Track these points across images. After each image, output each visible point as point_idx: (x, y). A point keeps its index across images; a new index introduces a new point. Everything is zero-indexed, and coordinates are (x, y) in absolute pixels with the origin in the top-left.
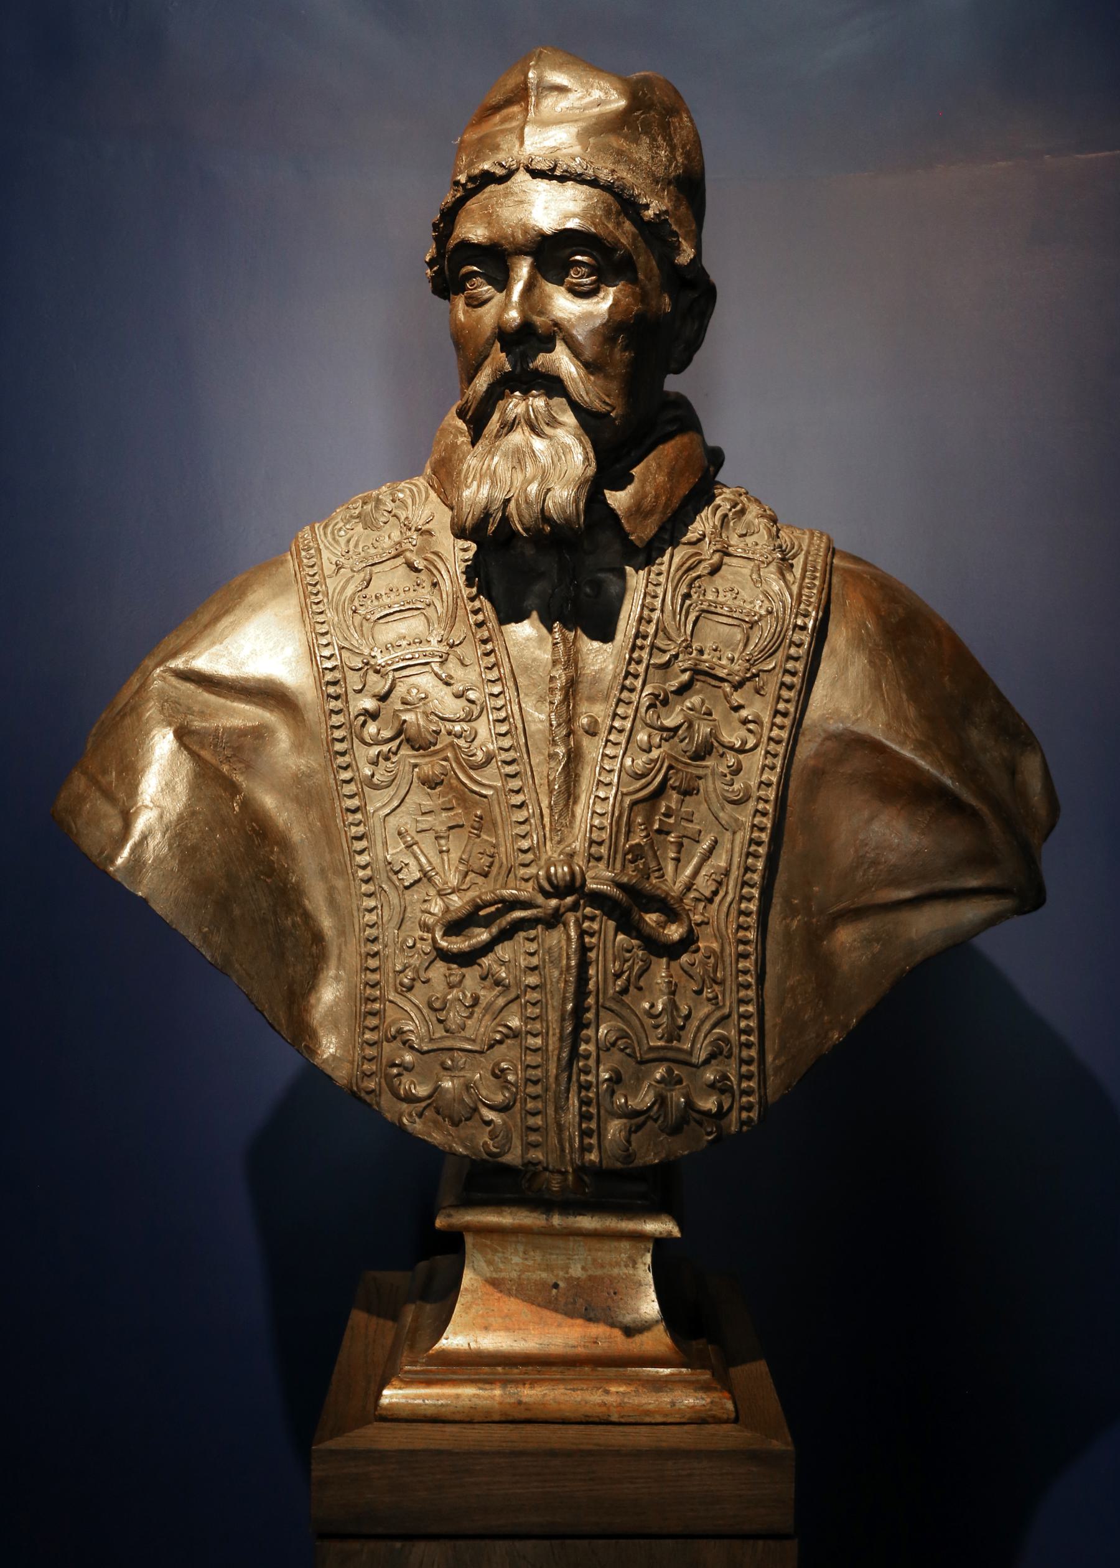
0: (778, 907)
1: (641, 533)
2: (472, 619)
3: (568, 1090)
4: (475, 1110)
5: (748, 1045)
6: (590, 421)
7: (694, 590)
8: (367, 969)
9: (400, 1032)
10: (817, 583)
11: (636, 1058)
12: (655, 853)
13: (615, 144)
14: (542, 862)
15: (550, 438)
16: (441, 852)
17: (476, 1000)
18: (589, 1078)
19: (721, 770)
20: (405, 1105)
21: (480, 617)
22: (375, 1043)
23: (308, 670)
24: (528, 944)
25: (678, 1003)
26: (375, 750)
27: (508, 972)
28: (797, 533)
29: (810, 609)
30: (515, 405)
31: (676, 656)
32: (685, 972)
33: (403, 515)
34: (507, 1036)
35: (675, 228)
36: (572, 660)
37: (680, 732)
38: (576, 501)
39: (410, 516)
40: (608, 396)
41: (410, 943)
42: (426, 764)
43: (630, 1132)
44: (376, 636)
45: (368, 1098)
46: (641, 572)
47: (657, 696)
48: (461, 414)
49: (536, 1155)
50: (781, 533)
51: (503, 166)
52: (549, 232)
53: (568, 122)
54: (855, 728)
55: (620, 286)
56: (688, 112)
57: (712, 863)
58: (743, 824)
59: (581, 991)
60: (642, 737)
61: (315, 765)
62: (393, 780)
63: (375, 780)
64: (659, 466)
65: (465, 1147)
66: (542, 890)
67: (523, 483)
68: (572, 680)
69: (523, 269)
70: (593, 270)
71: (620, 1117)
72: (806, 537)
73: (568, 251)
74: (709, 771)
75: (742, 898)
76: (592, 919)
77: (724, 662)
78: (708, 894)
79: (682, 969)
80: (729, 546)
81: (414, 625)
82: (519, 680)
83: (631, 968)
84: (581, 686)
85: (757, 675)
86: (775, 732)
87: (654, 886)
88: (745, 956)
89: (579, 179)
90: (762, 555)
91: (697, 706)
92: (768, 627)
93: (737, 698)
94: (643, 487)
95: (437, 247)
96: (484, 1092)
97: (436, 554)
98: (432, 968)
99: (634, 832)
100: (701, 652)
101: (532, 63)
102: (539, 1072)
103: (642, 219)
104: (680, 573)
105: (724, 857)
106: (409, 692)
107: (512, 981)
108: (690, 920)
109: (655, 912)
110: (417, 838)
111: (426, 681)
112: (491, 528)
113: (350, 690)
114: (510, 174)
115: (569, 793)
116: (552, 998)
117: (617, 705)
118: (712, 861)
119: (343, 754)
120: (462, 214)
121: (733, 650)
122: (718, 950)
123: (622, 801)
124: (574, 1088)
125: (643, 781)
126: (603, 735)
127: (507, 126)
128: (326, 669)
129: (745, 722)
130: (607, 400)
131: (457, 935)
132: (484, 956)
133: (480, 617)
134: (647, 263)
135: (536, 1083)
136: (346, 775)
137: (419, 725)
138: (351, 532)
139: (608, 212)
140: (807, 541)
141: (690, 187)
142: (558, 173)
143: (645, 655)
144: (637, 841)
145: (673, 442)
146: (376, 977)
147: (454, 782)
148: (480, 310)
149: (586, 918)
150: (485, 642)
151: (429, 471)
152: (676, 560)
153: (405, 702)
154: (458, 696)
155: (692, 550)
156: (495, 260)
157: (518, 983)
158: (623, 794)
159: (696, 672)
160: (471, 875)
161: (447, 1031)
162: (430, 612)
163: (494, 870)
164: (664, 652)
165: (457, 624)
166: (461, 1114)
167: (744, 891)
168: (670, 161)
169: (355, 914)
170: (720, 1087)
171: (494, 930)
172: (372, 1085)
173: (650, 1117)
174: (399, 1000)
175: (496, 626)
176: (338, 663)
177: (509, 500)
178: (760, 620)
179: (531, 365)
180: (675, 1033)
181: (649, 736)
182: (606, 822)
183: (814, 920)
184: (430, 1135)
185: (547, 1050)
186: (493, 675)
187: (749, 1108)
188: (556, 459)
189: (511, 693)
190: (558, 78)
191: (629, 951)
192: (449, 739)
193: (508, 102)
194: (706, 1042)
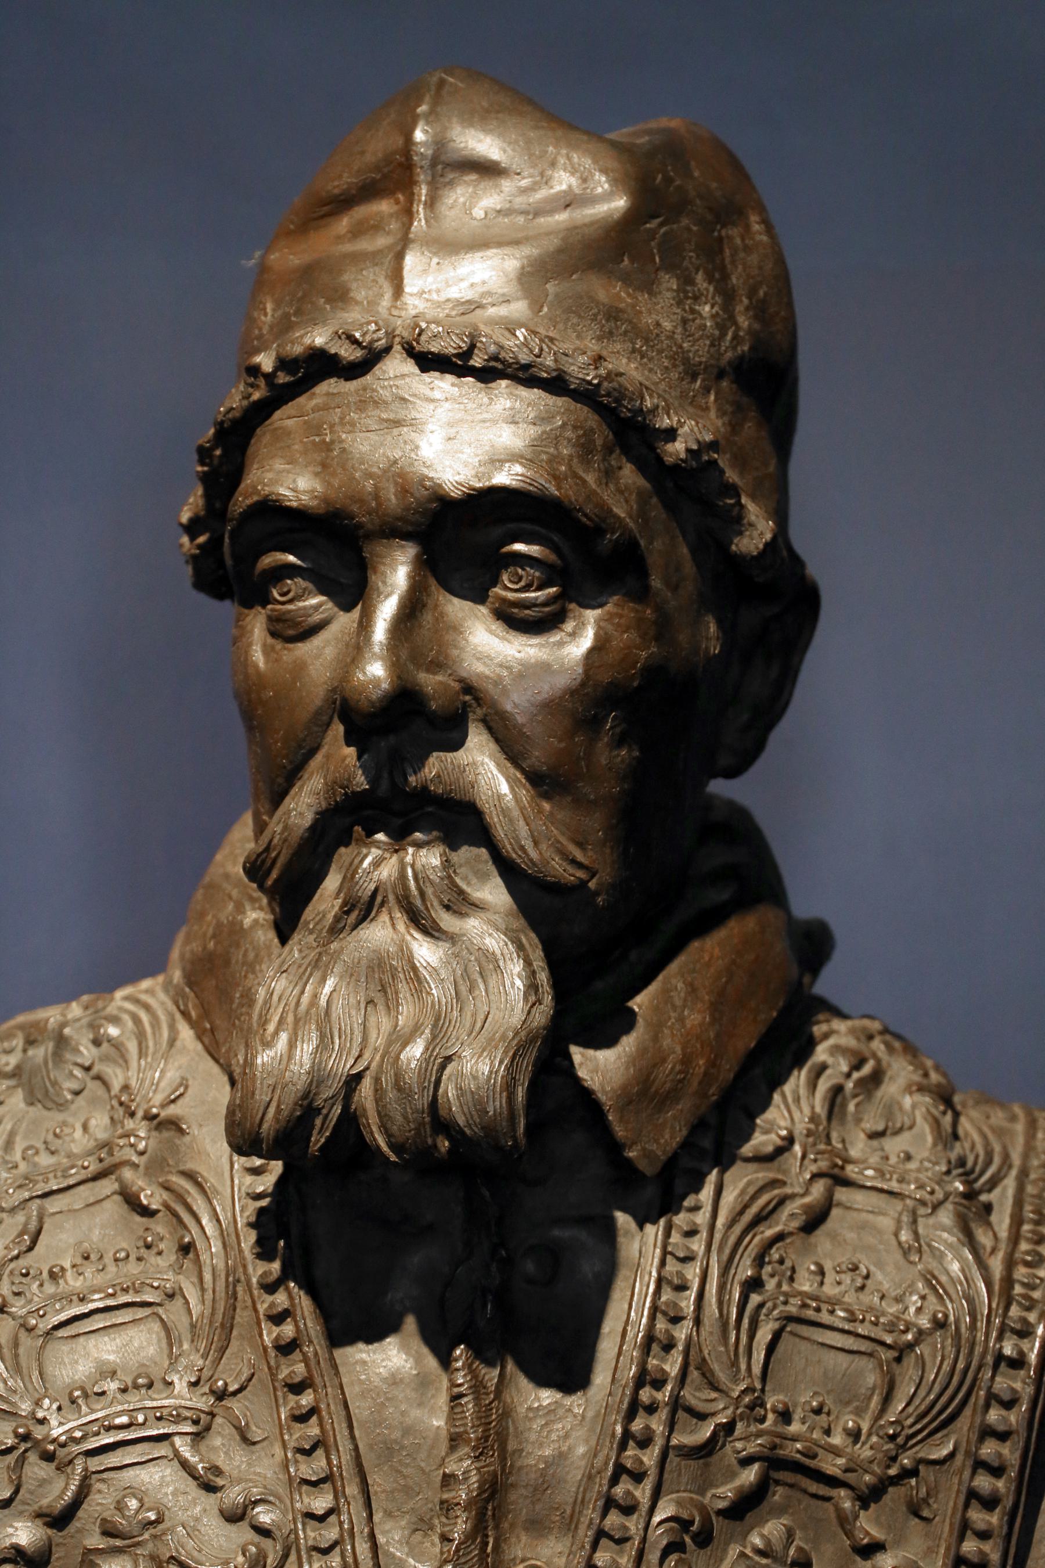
1: (650, 1143)
2: (269, 1334)
6: (539, 901)
7: (768, 1269)
13: (602, 295)
21: (288, 1330)
28: (998, 1117)
29: (1032, 1317)
30: (376, 862)
35: (732, 475)
36: (492, 1435)
38: (509, 1086)
39: (133, 1083)
40: (580, 845)
44: (49, 1369)
46: (650, 1229)
47: (684, 1524)
51: (355, 342)
52: (456, 494)
53: (500, 244)
55: (609, 607)
56: (761, 209)
64: (692, 989)
67: (389, 1043)
68: (494, 1483)
69: (397, 574)
70: (550, 574)
72: (1020, 1127)
73: (497, 531)
80: (847, 1161)
81: (134, 1345)
82: (377, 1480)
84: (513, 1496)
85: (913, 1472)
89: (524, 375)
91: (778, 1547)
92: (936, 1358)
93: (869, 1525)
94: (655, 1039)
95: (208, 496)
97: (190, 1176)
100: (785, 1416)
101: (423, 108)
103: (659, 460)
104: (738, 1229)
106: (120, 1507)
111: (158, 1480)
112: (318, 1140)
114: (372, 358)
120: (263, 440)
121: (859, 1412)
127: (365, 245)
130: (579, 856)
133: (288, 1330)
134: (668, 553)
139: (585, 449)
140: (1020, 1140)
141: (764, 383)
142: (477, 362)
143: (657, 1424)
145: (721, 934)
148: (303, 649)
150: (297, 1388)
151: (177, 975)
153: (109, 1531)
154: (234, 1516)
155: (762, 1174)
156: (337, 545)
159: (774, 1463)
162: (173, 1312)
164: (702, 1417)
168: (722, 328)
177: (358, 1077)
179: (412, 779)
186: (315, 1467)
188: (463, 989)
189: (356, 1510)
190: (484, 144)
193: (369, 191)
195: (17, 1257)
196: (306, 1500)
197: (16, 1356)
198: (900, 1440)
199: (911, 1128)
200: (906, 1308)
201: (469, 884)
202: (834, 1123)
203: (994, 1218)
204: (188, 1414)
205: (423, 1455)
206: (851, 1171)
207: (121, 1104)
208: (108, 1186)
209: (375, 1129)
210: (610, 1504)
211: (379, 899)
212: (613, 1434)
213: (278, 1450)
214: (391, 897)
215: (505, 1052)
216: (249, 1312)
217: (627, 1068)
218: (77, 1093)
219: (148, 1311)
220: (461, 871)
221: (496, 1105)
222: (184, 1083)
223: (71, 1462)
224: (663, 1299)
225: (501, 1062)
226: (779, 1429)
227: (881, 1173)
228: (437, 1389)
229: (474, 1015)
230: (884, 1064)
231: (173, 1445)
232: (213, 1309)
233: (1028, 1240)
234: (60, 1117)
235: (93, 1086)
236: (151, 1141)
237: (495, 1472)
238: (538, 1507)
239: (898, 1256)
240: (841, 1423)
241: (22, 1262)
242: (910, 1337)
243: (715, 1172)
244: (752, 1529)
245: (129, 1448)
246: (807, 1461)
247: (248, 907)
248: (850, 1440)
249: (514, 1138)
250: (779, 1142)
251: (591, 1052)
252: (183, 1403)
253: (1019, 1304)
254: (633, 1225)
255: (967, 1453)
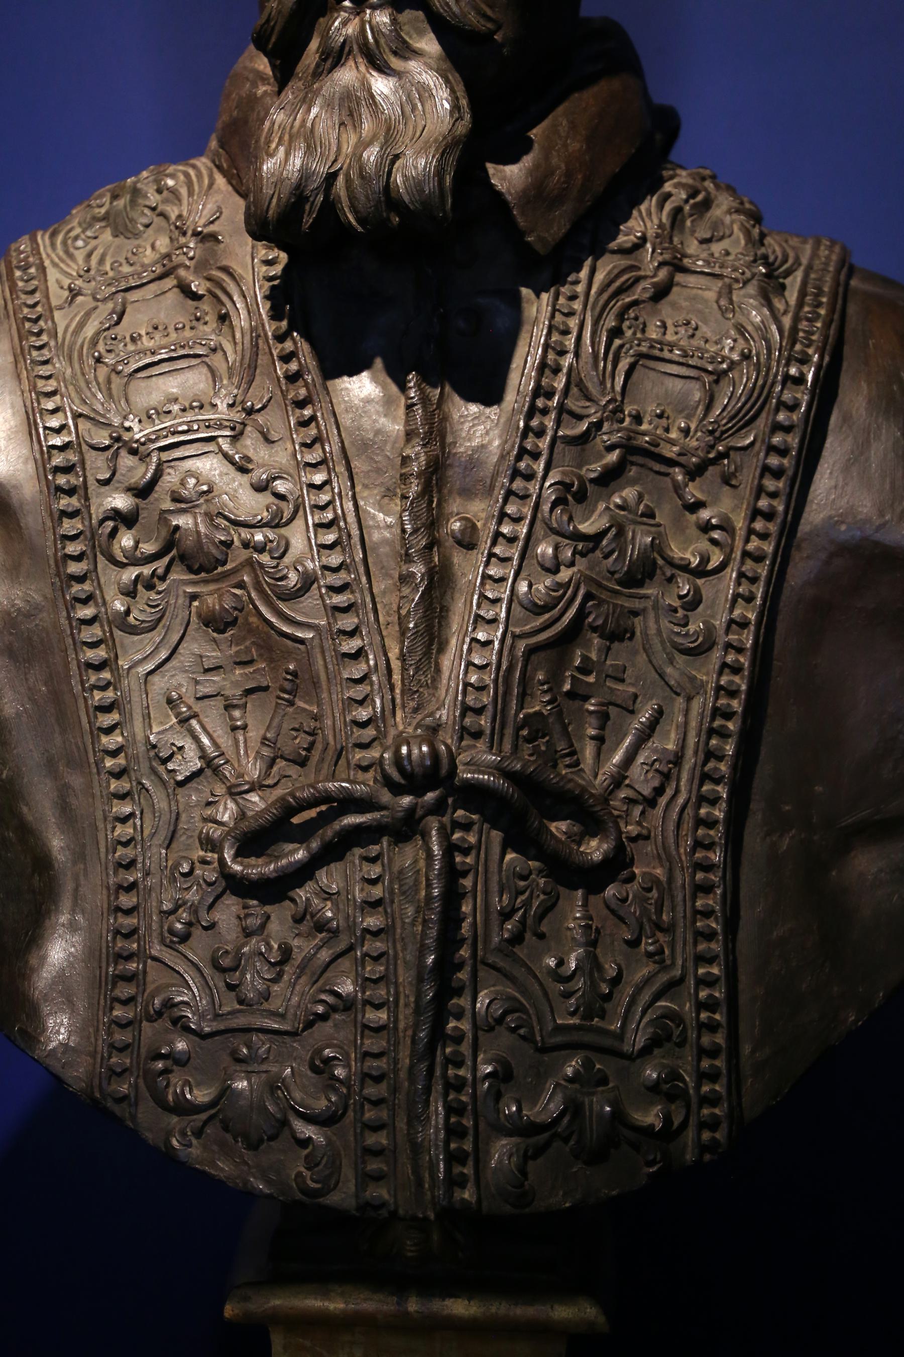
0: (759, 816)
1: (545, 232)
3: (428, 1090)
4: (284, 1123)
5: (712, 1027)
7: (627, 323)
8: (118, 909)
9: (169, 1004)
10: (822, 312)
11: (535, 1042)
12: (565, 727)
14: (390, 741)
15: (397, 74)
16: (234, 729)
17: (286, 953)
18: (461, 1072)
19: (668, 601)
20: (175, 1119)
21: (294, 366)
22: (130, 1023)
23: (26, 451)
24: (366, 866)
25: (601, 960)
26: (130, 574)
27: (336, 909)
28: (794, 241)
29: (810, 351)
31: (598, 425)
32: (613, 912)
33: (173, 214)
34: (333, 1009)
36: (435, 431)
37: (604, 542)
38: (440, 173)
39: (185, 213)
40: (491, 7)
41: (185, 868)
42: (211, 594)
43: (526, 1158)
44: (132, 398)
45: (117, 1109)
46: (545, 296)
48: (261, 44)
49: (381, 1192)
50: (768, 240)
54: (878, 537)
57: (651, 747)
58: (703, 685)
59: (449, 939)
60: (545, 549)
61: (37, 598)
62: (159, 620)
63: (131, 619)
64: (573, 126)
65: (268, 1182)
66: (388, 782)
67: (356, 147)
71: (510, 1134)
74: (649, 604)
75: (702, 799)
76: (466, 827)
77: (673, 435)
78: (647, 791)
79: (608, 907)
80: (685, 256)
81: (189, 382)
82: (355, 463)
83: (527, 904)
84: (450, 473)
86: (754, 544)
87: (563, 777)
88: (706, 889)
90: (735, 270)
92: (744, 380)
96: (298, 1095)
98: (219, 905)
99: (532, 695)
100: (638, 419)
102: (382, 1064)
104: (605, 296)
105: (673, 735)
106: (183, 483)
107: (342, 923)
108: (620, 832)
109: (565, 819)
110: (197, 707)
111: (209, 466)
112: (308, 221)
113: (91, 481)
115: (431, 634)
116: (404, 949)
117: (506, 501)
118: (655, 743)
119: (81, 579)
121: (689, 417)
122: (663, 879)
123: (513, 647)
124: (438, 1087)
125: (547, 616)
126: (485, 546)
128: (54, 447)
129: (706, 528)
130: (489, 12)
131: (258, 856)
132: (300, 887)
133: (294, 366)
135: (378, 1079)
136: (87, 612)
137: (198, 533)
138: (93, 243)
143: (550, 423)
144: (537, 708)
145: (595, 89)
146: (130, 922)
147: (253, 620)
149: (457, 825)
150: (301, 404)
151: (213, 144)
152: (600, 277)
153: (177, 498)
154: (260, 488)
155: (623, 262)
157: (351, 927)
158: (515, 637)
159: (631, 450)
160: (281, 763)
161: (241, 1002)
162: (217, 360)
163: (316, 755)
164: (580, 418)
165: (258, 378)
166: (262, 1130)
167: (705, 788)
169: (101, 825)
170: (667, 1090)
171: (315, 845)
172: (124, 1089)
173: (556, 1135)
174: (168, 956)
175: (319, 381)
176: (73, 437)
177: (335, 175)
178: (730, 369)
180: (596, 1006)
181: (556, 548)
182: (488, 678)
183: (816, 838)
184: (213, 1164)
185: (396, 1028)
186: (313, 456)
187: (713, 1124)
188: (408, 109)
189: (340, 483)
191: (524, 878)
192: (244, 554)
194: (645, 1020)
195: (108, 329)
196: (309, 476)
197: (109, 389)
198: (717, 434)
199: (730, 236)
200: (723, 348)
201: (410, 37)
202: (676, 232)
203: (787, 293)
204: (227, 424)
205: (388, 448)
206: (686, 262)
207: (177, 227)
208: (170, 282)
209: (346, 210)
210: (516, 473)
211: (347, 49)
212: (518, 427)
213: (289, 446)
214: (355, 47)
215: (437, 150)
216: (268, 356)
217: (527, 177)
218: (147, 226)
219: (198, 361)
220: (406, 28)
221: (430, 187)
222: (219, 210)
223: (149, 454)
224: (553, 339)
225: (433, 157)
226: (634, 427)
227: (707, 263)
228: (398, 406)
229: (415, 127)
230: (713, 196)
231: (218, 444)
232: (243, 356)
233: (809, 305)
234: (136, 242)
235: (158, 221)
236: (198, 251)
237: (437, 456)
238: (467, 480)
239: (719, 315)
240: (677, 424)
241: (111, 331)
242: (725, 366)
243: (590, 259)
244: (614, 493)
245: (188, 446)
246: (653, 449)
247: (259, 83)
248: (682, 435)
249: (444, 212)
250: (635, 240)
251: (501, 167)
252: (224, 417)
253: (802, 343)
254: (533, 296)
255: (763, 441)
